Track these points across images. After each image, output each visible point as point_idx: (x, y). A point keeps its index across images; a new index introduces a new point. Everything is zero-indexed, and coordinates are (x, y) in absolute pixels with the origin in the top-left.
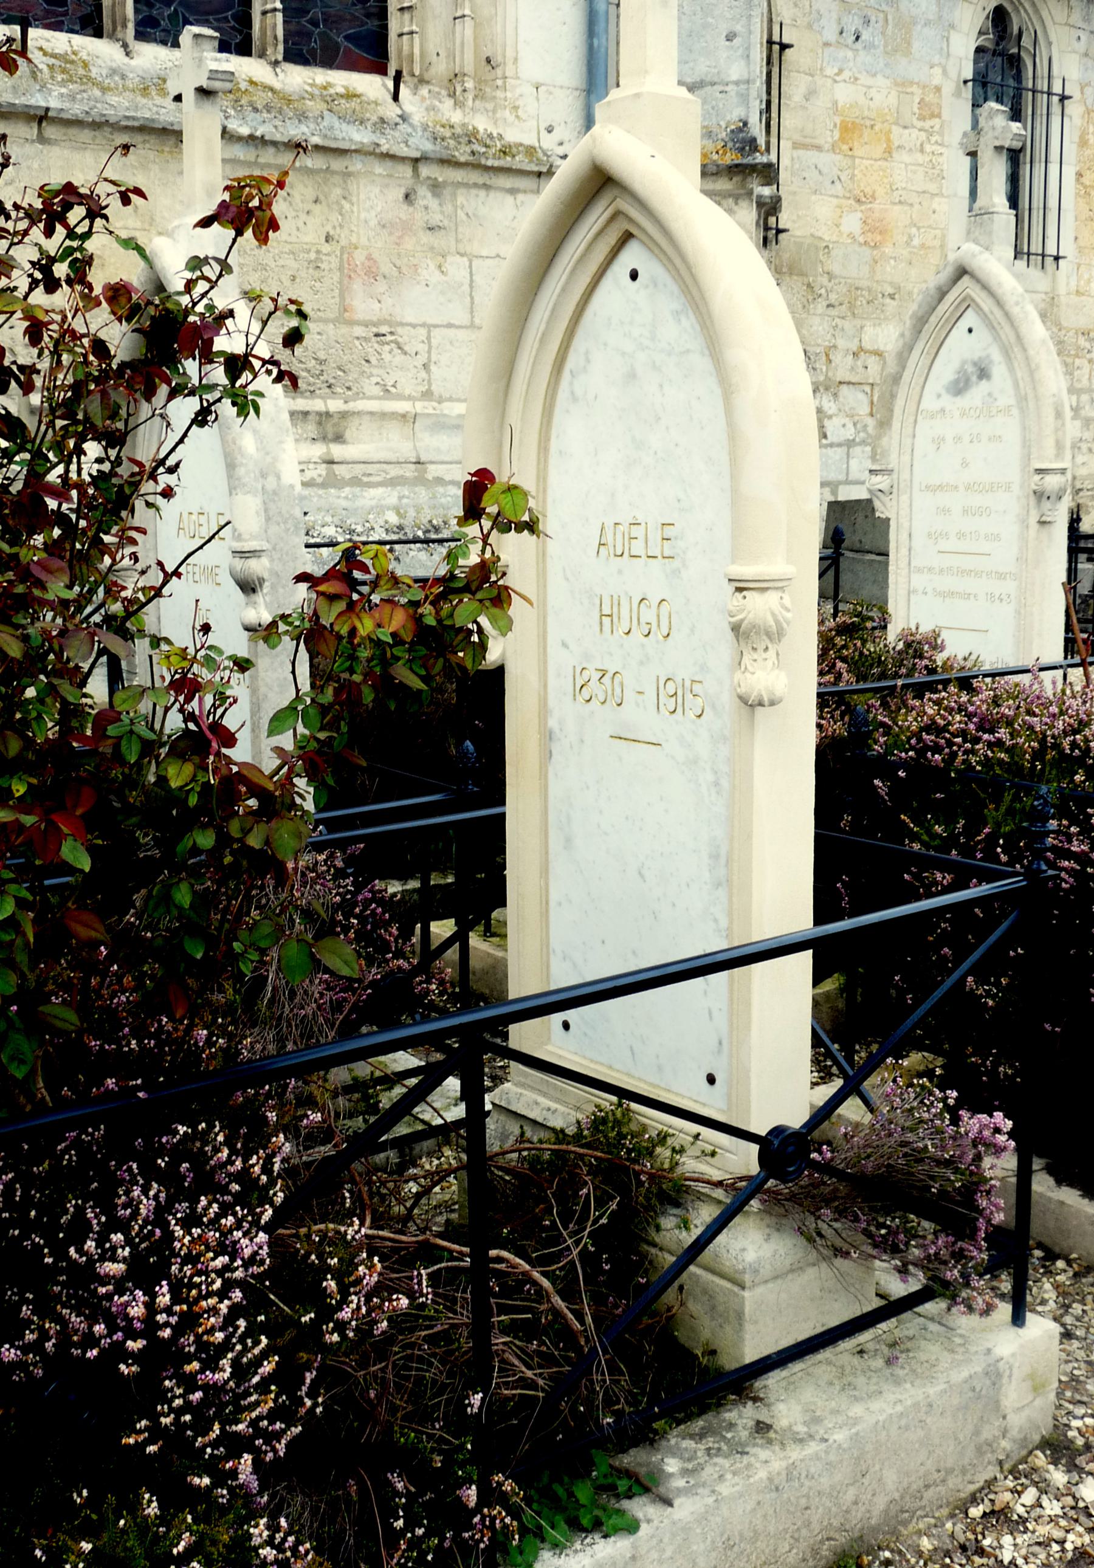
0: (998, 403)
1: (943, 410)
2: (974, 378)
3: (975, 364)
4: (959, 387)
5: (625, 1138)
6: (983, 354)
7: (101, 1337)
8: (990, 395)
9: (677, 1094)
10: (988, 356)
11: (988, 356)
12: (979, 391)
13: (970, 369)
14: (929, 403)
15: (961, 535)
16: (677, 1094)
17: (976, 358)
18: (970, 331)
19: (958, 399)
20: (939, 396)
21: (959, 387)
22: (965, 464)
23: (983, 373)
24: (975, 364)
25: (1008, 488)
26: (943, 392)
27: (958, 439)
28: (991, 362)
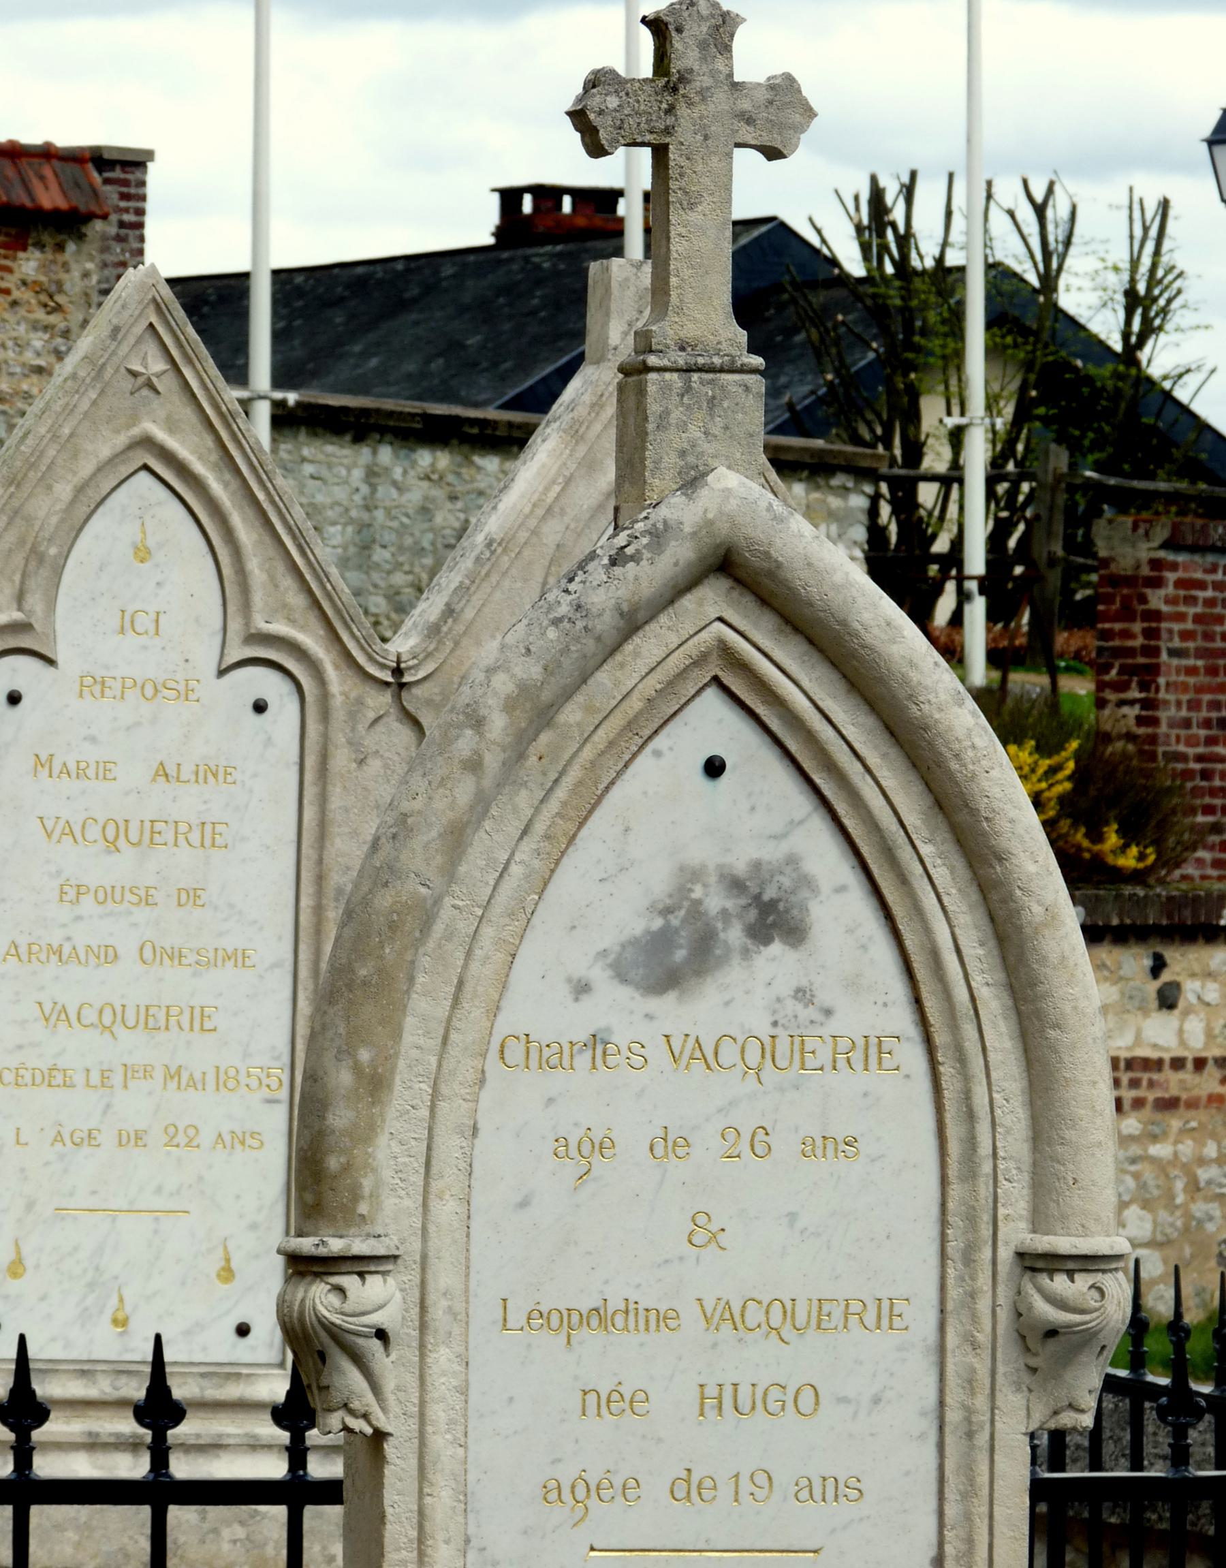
0: (834, 1026)
1: (597, 1042)
2: (734, 935)
3: (736, 885)
4: (672, 957)
5: (1144, 687)
6: (771, 853)
7: (377, 566)
8: (803, 994)
9: (809, 1316)
10: (792, 860)
11: (792, 860)
12: (753, 986)
13: (715, 901)
14: (536, 1004)
15: (689, 1488)
16: (809, 1316)
17: (740, 867)
18: (714, 768)
19: (666, 1005)
20: (582, 988)
21: (672, 957)
22: (704, 1233)
23: (773, 917)
24: (736, 885)
25: (887, 1314)
26: (599, 976)
27: (669, 1145)
28: (806, 882)
